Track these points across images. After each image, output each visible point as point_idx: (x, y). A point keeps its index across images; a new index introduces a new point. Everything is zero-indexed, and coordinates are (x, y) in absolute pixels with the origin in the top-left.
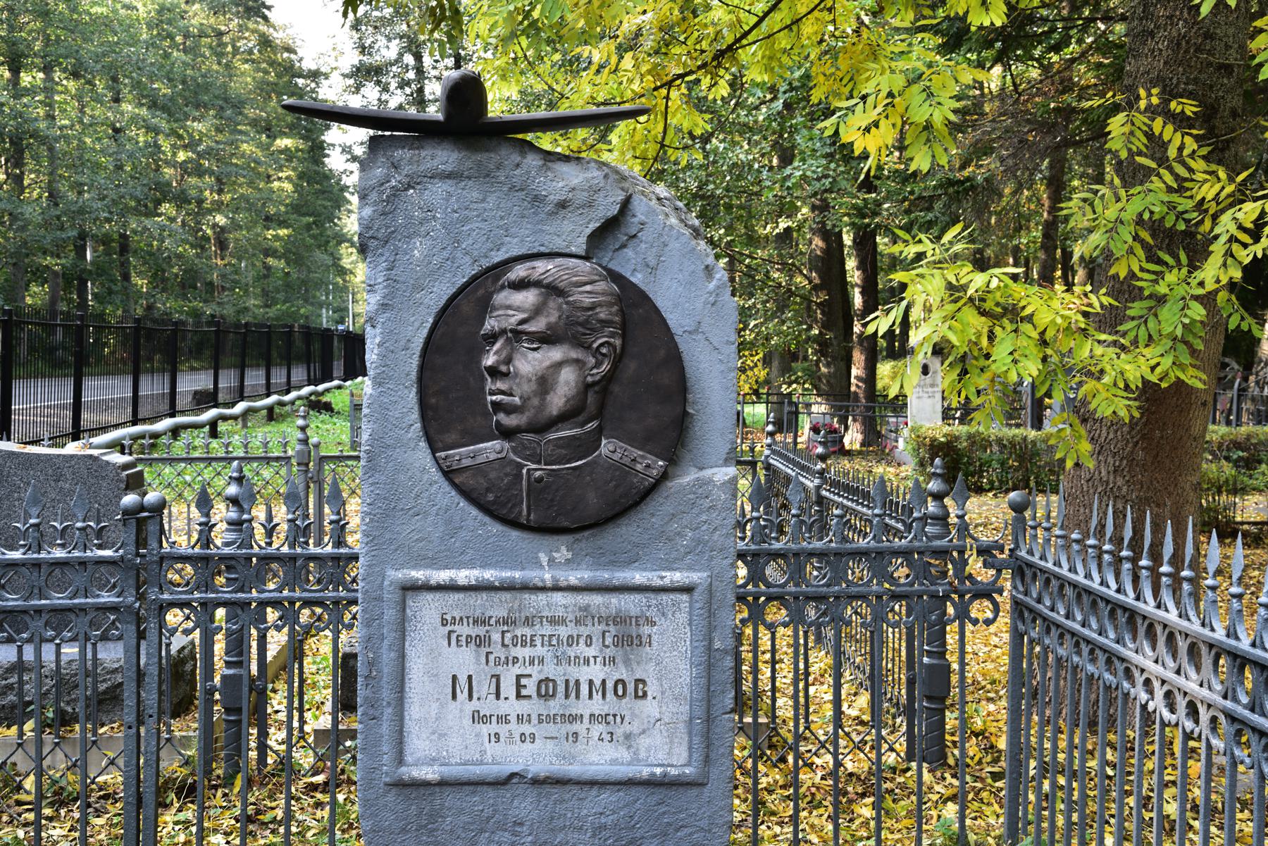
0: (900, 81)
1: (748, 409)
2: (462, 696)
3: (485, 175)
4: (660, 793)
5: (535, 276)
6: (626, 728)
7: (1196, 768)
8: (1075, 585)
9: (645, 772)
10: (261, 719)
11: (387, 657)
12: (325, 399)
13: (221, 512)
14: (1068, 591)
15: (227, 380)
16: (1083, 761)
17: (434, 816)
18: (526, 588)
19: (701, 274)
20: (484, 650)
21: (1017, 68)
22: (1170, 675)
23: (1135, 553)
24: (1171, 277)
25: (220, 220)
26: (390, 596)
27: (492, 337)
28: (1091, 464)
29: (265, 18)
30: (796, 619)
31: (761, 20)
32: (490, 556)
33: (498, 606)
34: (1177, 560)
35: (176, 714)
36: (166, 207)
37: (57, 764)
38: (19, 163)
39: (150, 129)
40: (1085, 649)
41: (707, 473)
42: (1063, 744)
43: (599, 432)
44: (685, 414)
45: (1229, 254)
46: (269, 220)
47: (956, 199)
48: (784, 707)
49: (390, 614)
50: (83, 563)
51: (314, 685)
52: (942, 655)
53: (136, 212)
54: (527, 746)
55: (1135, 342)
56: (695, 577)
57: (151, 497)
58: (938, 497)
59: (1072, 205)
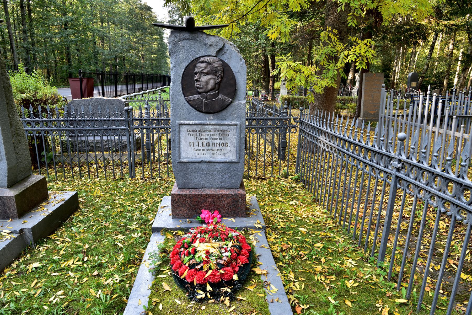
0: (279, 23)
1: (249, 92)
2: (192, 146)
3: (195, 39)
4: (230, 164)
5: (205, 60)
6: (224, 152)
7: (331, 160)
8: (311, 125)
9: (228, 160)
10: (154, 151)
11: (177, 138)
12: (164, 89)
13: (144, 111)
14: (310, 126)
15: (145, 86)
16: (311, 159)
17: (187, 169)
18: (204, 125)
19: (239, 60)
21: (304, 23)
22: (328, 142)
23: (323, 119)
24: (331, 65)
25: (143, 53)
26: (177, 126)
27: (196, 73)
28: (314, 102)
29: (151, 11)
30: (257, 132)
31: (252, 9)
32: (195, 118)
33: (198, 128)
34: (330, 120)
35: (137, 150)
36: (132, 51)
37: (116, 159)
38: (103, 42)
39: (128, 34)
40: (312, 137)
41: (240, 102)
42: (307, 156)
43: (218, 93)
44: (236, 89)
45: (342, 61)
46: (152, 53)
47: (291, 49)
48: (255, 150)
49: (177, 130)
50: (118, 120)
51: (164, 145)
52: (285, 139)
53: (126, 52)
54: (205, 155)
55: (324, 78)
56: (237, 123)
57: (130, 107)
58: (286, 108)
59: (313, 50)
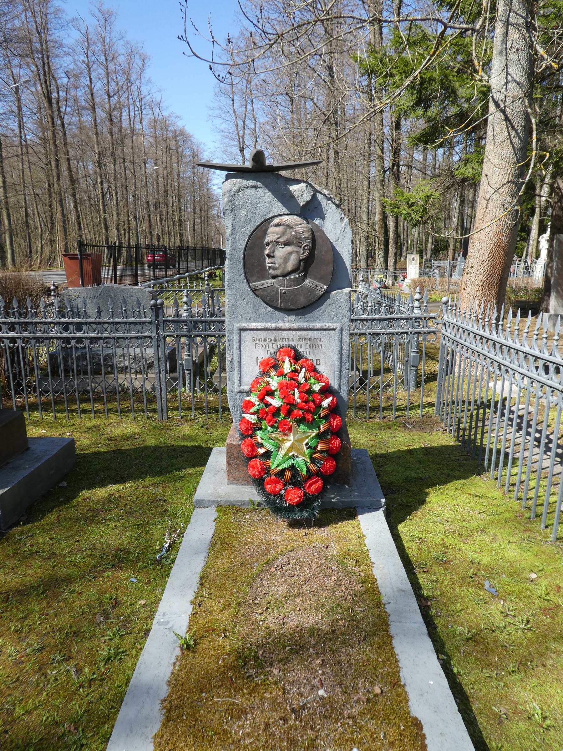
18: (280, 329)
20: (267, 350)
43: (305, 277)
